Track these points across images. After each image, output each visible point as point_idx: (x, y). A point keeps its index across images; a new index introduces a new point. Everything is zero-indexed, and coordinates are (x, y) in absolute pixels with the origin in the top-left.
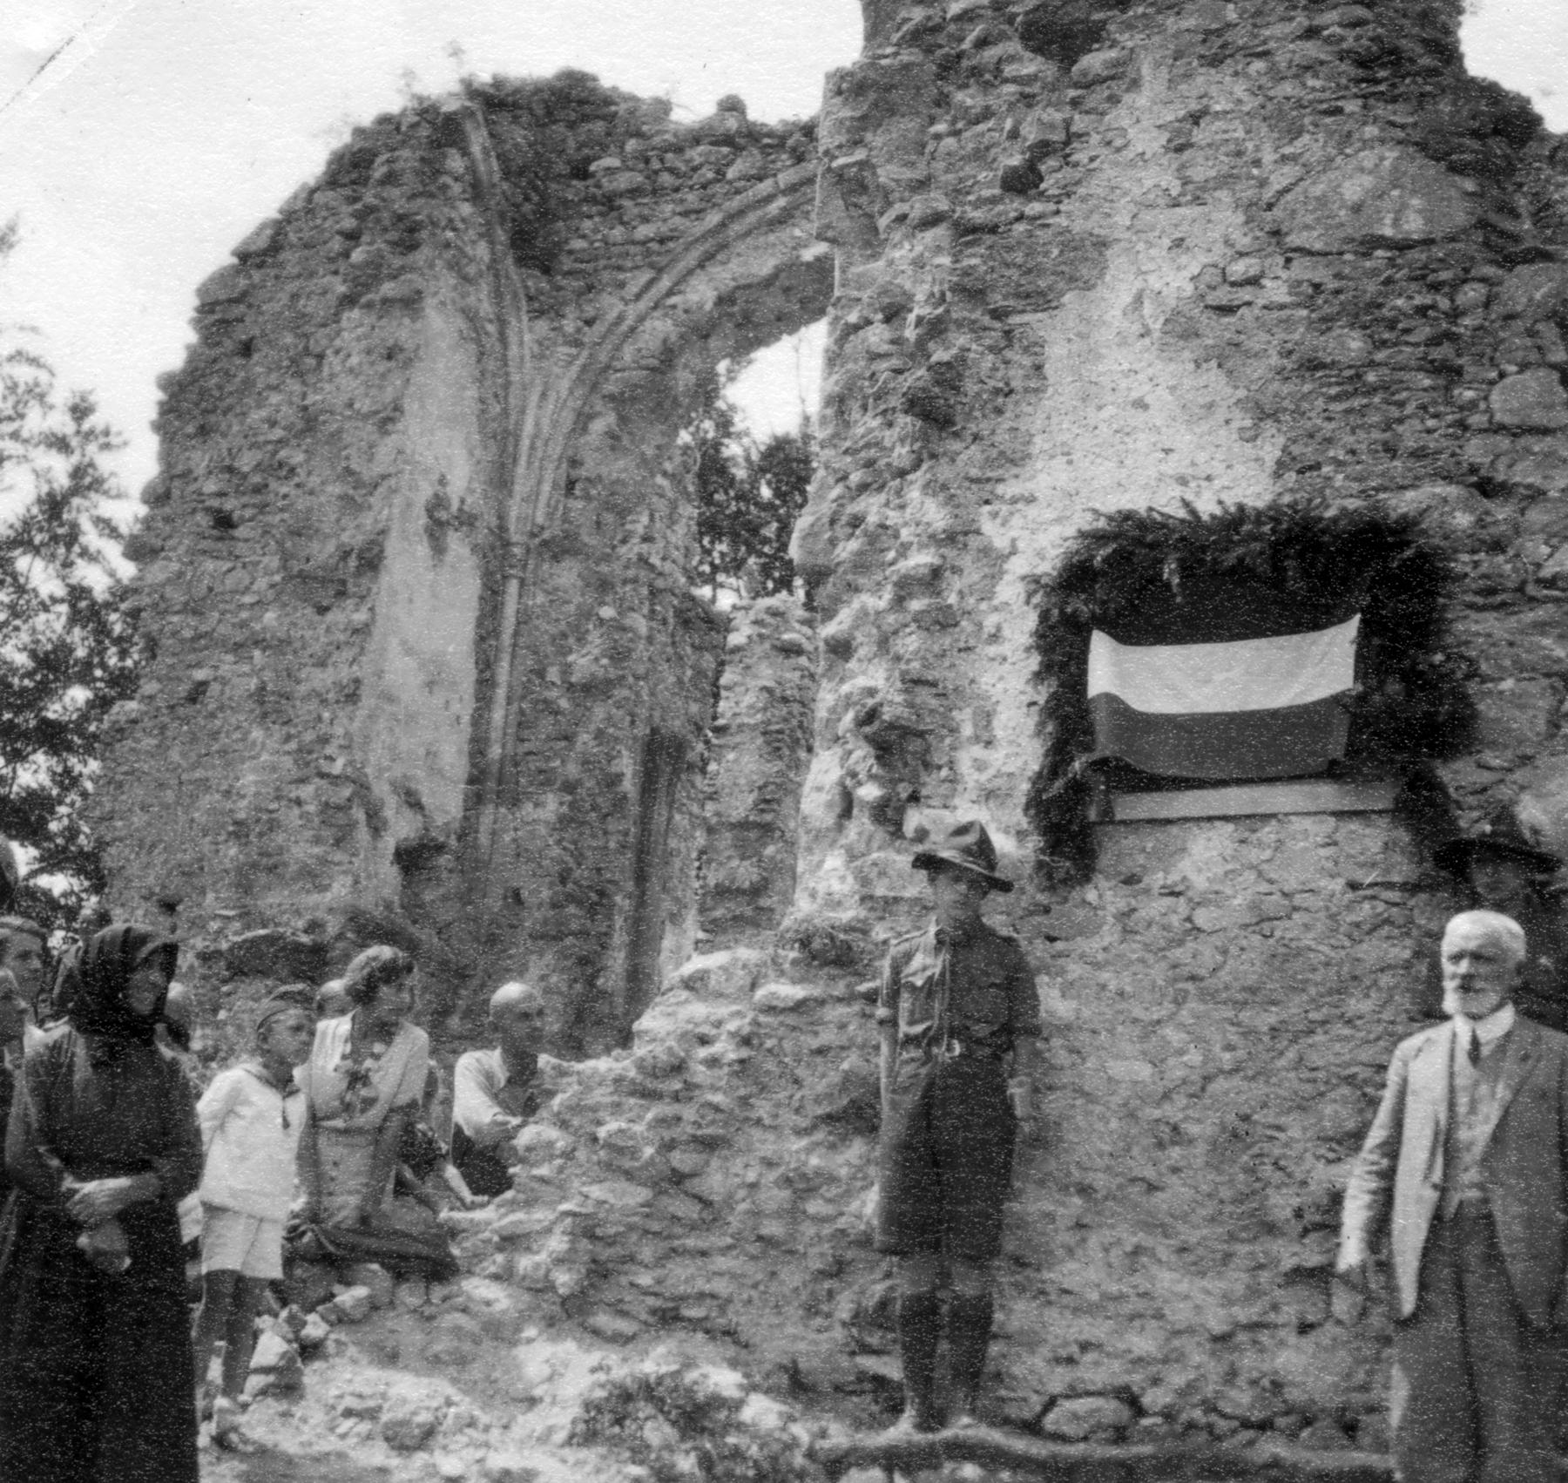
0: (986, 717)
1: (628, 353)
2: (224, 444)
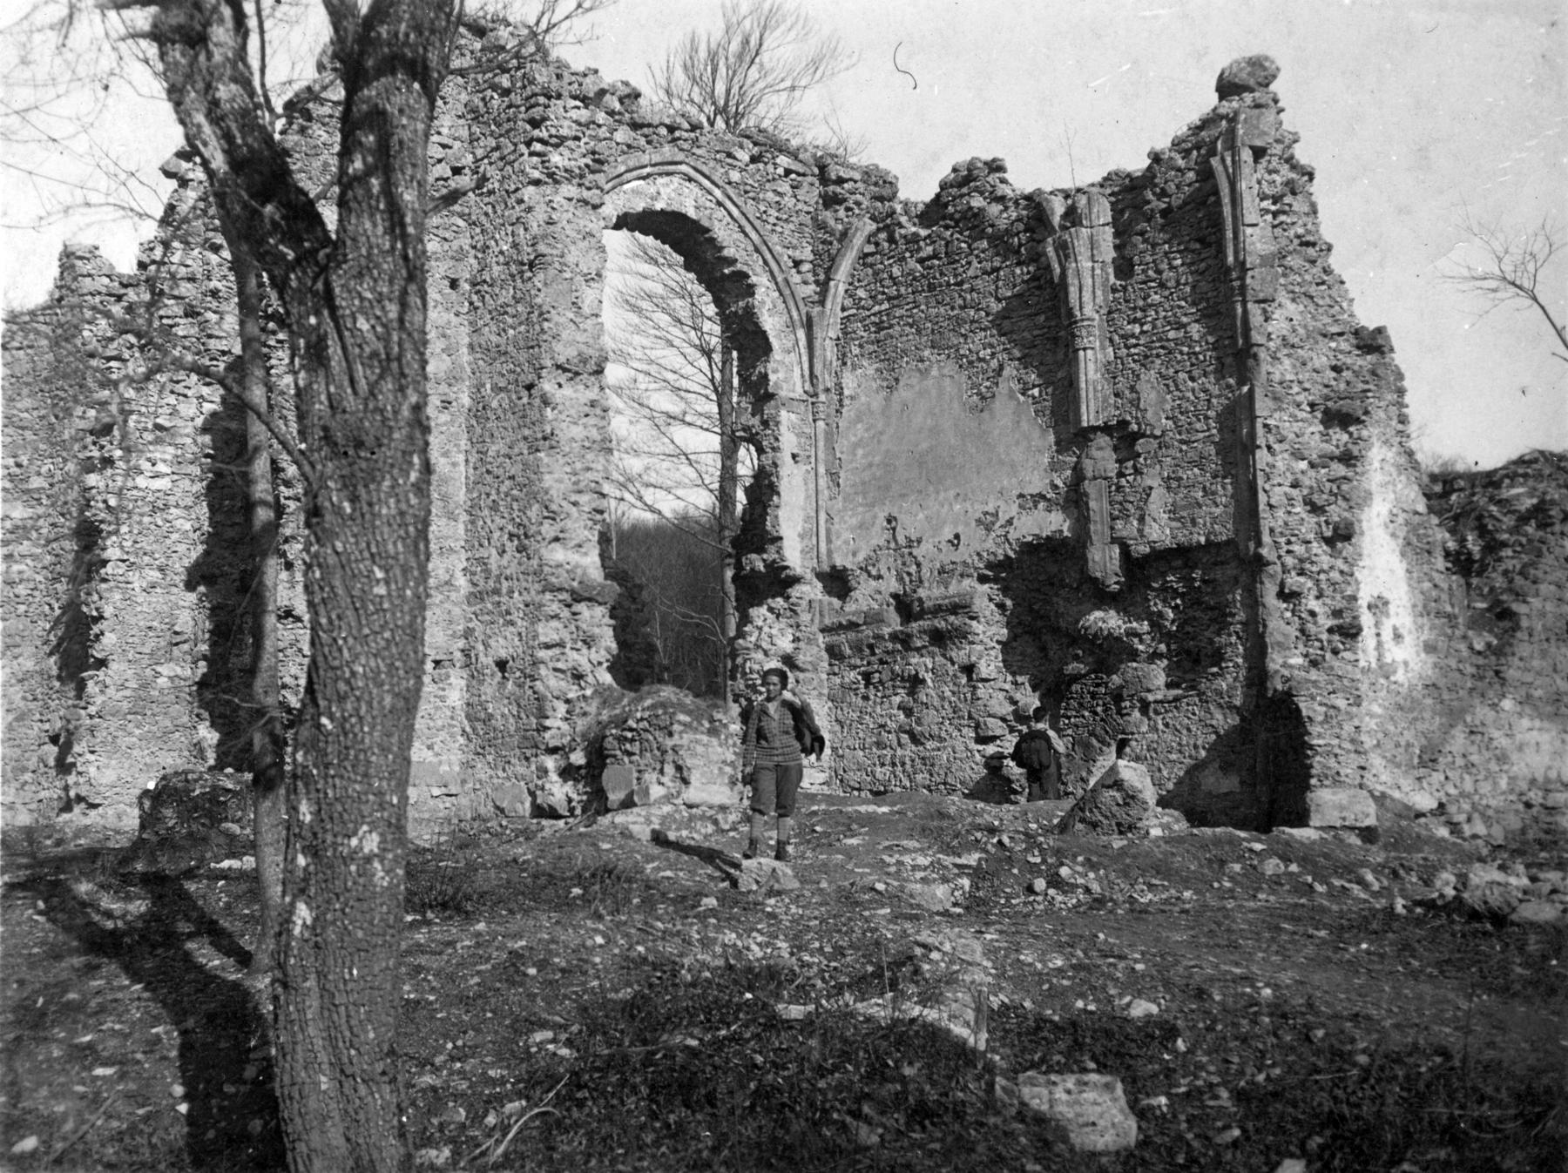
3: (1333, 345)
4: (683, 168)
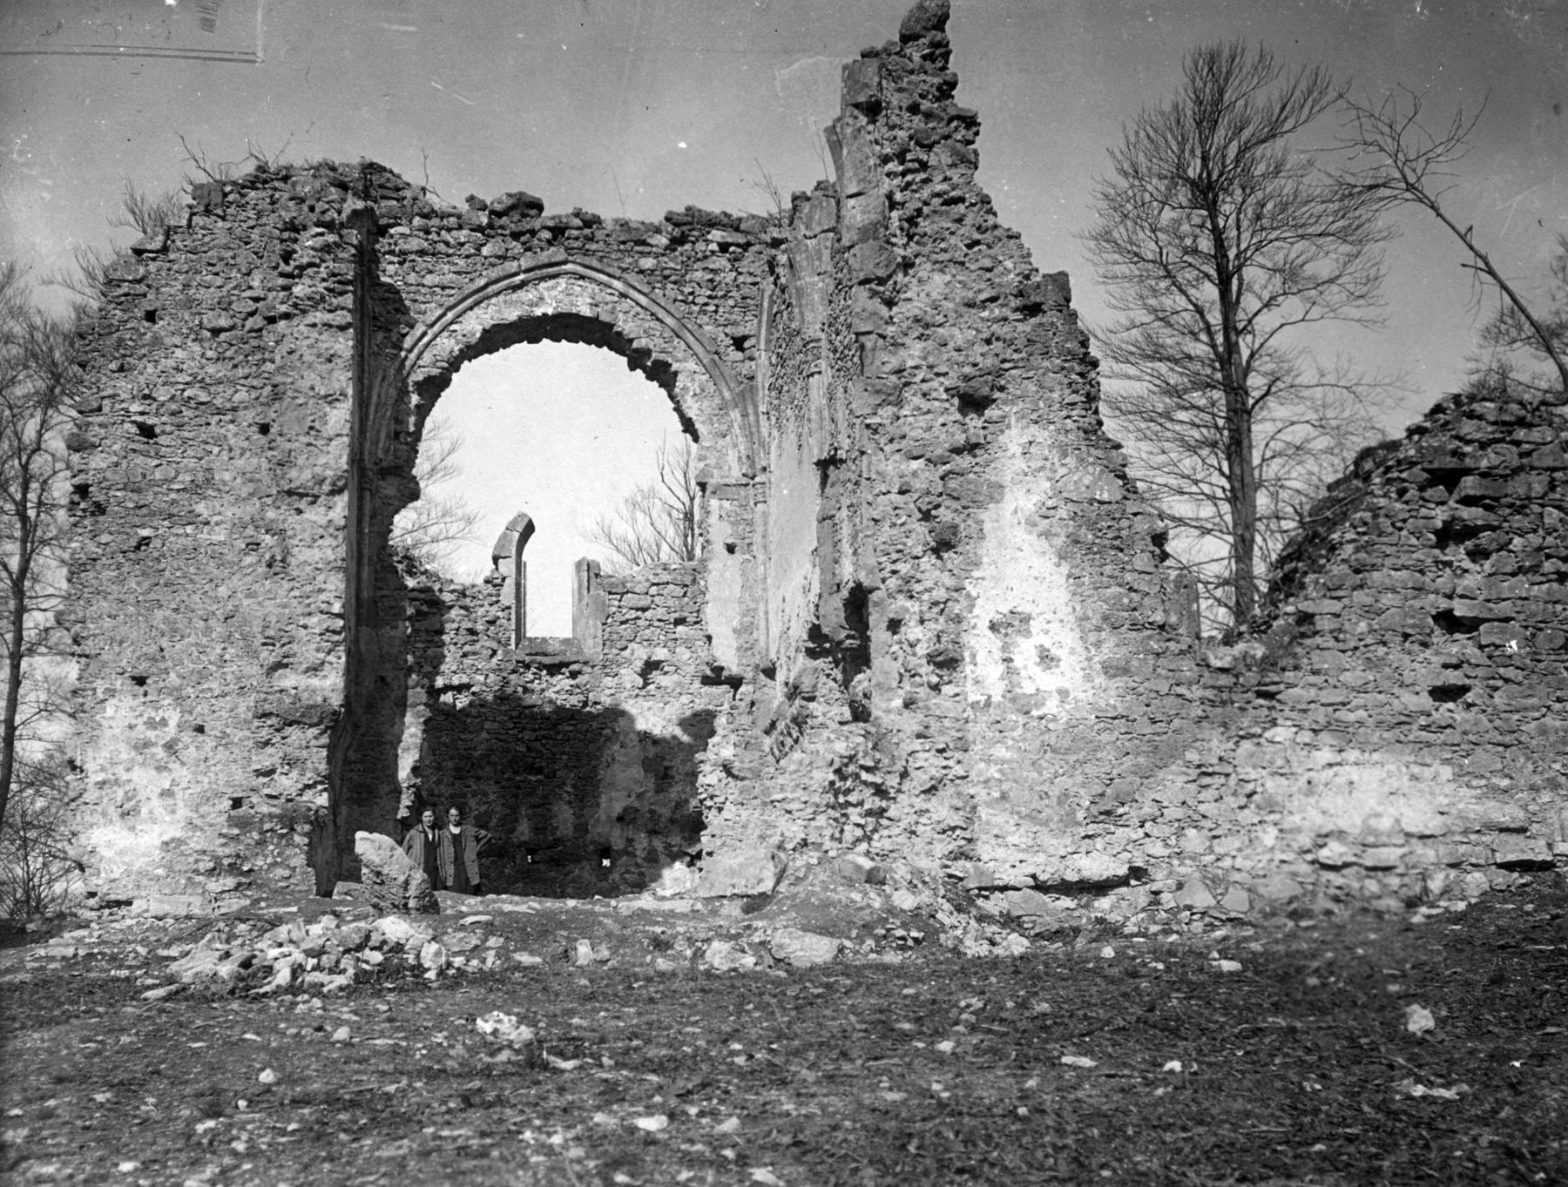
0: (974, 656)
1: (427, 358)
2: (142, 379)
3: (985, 314)
4: (569, 267)
